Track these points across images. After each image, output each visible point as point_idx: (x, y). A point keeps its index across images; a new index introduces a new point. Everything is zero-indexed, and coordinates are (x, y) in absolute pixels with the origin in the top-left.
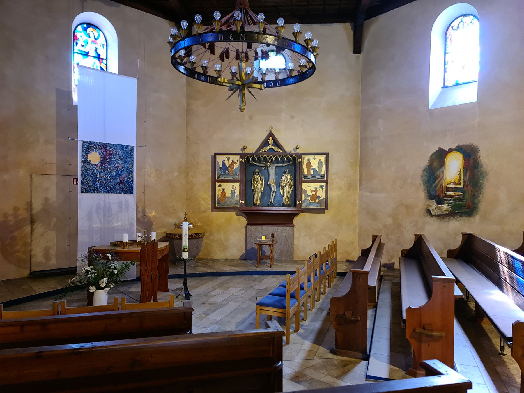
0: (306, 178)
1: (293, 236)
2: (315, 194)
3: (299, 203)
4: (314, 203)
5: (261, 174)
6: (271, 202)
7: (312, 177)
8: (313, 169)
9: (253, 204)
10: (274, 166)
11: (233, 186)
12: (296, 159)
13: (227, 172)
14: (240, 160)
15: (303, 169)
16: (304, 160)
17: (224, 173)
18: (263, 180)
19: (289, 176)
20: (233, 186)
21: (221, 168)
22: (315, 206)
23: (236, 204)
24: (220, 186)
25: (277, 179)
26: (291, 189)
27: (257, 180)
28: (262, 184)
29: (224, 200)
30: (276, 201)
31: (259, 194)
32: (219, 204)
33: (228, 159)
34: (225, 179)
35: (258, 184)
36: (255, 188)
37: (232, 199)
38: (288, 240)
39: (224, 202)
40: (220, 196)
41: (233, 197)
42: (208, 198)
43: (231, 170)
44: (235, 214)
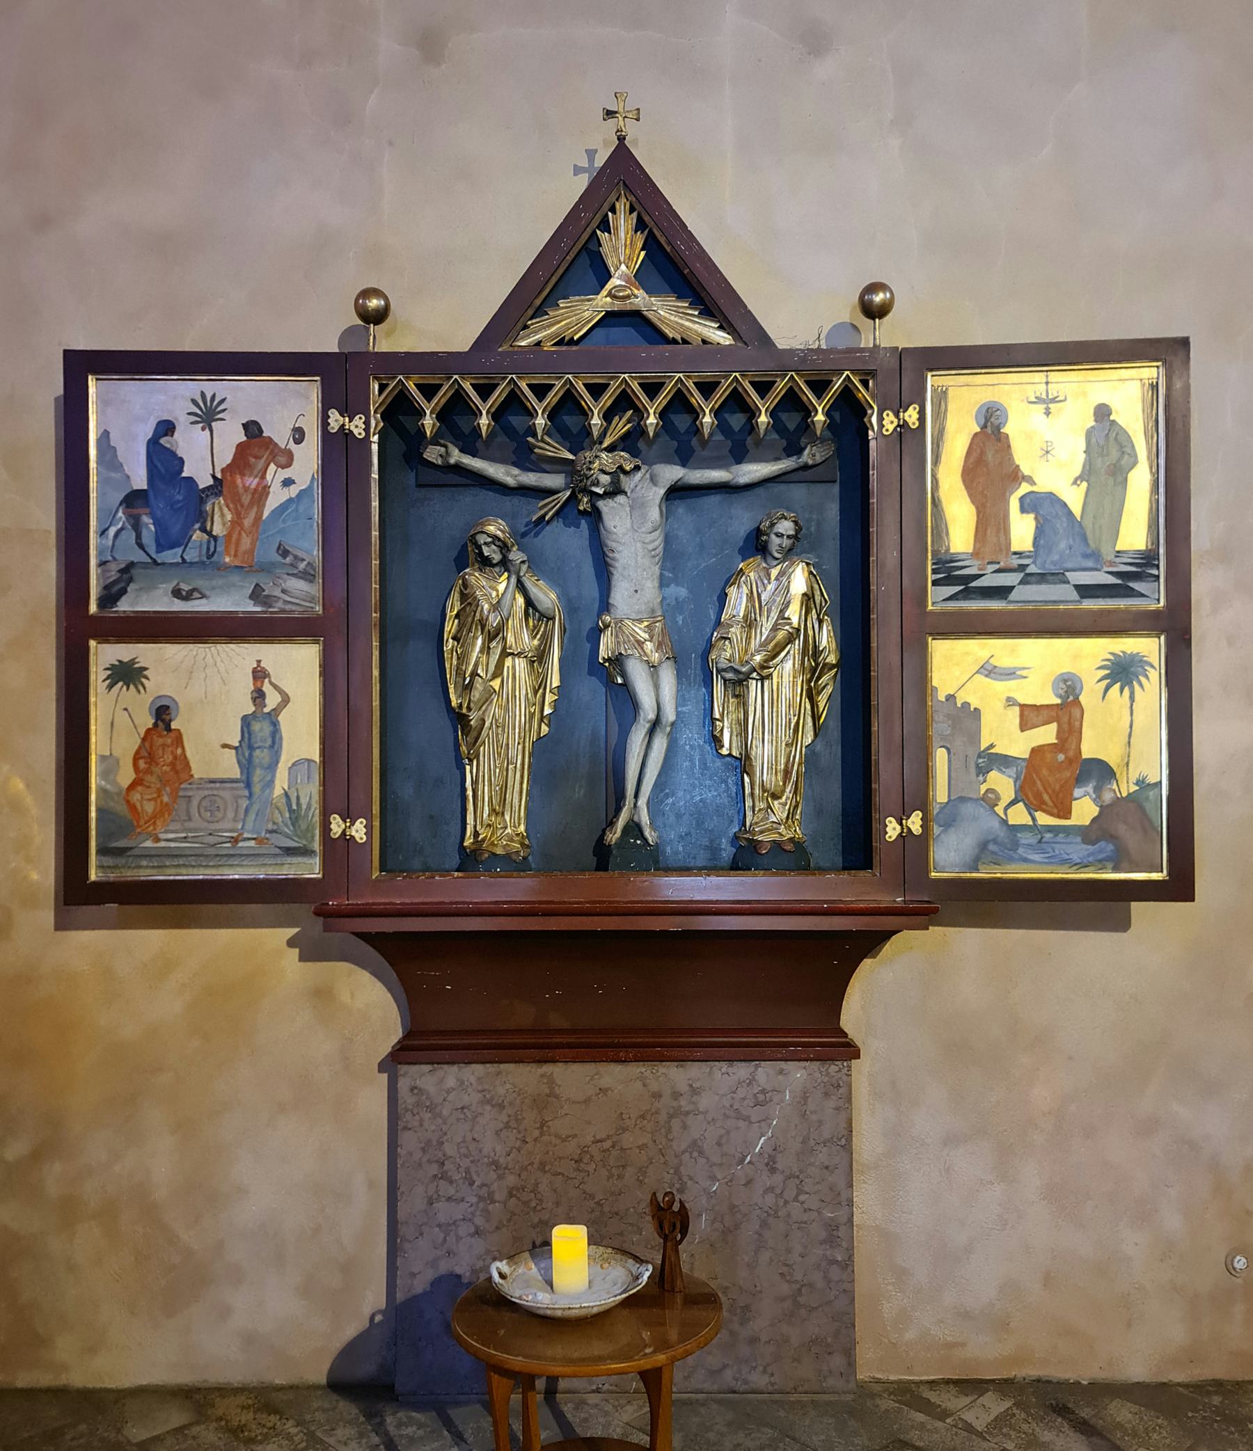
0: (967, 594)
1: (848, 1148)
2: (1060, 746)
3: (906, 836)
4: (1050, 829)
6: (634, 828)
7: (1027, 579)
9: (462, 847)
10: (654, 480)
11: (259, 674)
13: (197, 536)
15: (936, 503)
16: (940, 415)
17: (172, 547)
18: (553, 618)
19: (799, 581)
20: (259, 674)
21: (134, 499)
22: (1064, 862)
23: (289, 851)
24: (127, 674)
25: (679, 606)
27: (494, 620)
28: (540, 657)
29: (163, 811)
30: (679, 816)
31: (519, 756)
32: (121, 852)
33: (208, 415)
34: (179, 606)
35: (505, 654)
36: (476, 694)
37: (244, 803)
38: (800, 1191)
39: (169, 837)
40: (126, 776)
41: (257, 789)
42: (29, 800)
43: (237, 523)
44: (291, 943)
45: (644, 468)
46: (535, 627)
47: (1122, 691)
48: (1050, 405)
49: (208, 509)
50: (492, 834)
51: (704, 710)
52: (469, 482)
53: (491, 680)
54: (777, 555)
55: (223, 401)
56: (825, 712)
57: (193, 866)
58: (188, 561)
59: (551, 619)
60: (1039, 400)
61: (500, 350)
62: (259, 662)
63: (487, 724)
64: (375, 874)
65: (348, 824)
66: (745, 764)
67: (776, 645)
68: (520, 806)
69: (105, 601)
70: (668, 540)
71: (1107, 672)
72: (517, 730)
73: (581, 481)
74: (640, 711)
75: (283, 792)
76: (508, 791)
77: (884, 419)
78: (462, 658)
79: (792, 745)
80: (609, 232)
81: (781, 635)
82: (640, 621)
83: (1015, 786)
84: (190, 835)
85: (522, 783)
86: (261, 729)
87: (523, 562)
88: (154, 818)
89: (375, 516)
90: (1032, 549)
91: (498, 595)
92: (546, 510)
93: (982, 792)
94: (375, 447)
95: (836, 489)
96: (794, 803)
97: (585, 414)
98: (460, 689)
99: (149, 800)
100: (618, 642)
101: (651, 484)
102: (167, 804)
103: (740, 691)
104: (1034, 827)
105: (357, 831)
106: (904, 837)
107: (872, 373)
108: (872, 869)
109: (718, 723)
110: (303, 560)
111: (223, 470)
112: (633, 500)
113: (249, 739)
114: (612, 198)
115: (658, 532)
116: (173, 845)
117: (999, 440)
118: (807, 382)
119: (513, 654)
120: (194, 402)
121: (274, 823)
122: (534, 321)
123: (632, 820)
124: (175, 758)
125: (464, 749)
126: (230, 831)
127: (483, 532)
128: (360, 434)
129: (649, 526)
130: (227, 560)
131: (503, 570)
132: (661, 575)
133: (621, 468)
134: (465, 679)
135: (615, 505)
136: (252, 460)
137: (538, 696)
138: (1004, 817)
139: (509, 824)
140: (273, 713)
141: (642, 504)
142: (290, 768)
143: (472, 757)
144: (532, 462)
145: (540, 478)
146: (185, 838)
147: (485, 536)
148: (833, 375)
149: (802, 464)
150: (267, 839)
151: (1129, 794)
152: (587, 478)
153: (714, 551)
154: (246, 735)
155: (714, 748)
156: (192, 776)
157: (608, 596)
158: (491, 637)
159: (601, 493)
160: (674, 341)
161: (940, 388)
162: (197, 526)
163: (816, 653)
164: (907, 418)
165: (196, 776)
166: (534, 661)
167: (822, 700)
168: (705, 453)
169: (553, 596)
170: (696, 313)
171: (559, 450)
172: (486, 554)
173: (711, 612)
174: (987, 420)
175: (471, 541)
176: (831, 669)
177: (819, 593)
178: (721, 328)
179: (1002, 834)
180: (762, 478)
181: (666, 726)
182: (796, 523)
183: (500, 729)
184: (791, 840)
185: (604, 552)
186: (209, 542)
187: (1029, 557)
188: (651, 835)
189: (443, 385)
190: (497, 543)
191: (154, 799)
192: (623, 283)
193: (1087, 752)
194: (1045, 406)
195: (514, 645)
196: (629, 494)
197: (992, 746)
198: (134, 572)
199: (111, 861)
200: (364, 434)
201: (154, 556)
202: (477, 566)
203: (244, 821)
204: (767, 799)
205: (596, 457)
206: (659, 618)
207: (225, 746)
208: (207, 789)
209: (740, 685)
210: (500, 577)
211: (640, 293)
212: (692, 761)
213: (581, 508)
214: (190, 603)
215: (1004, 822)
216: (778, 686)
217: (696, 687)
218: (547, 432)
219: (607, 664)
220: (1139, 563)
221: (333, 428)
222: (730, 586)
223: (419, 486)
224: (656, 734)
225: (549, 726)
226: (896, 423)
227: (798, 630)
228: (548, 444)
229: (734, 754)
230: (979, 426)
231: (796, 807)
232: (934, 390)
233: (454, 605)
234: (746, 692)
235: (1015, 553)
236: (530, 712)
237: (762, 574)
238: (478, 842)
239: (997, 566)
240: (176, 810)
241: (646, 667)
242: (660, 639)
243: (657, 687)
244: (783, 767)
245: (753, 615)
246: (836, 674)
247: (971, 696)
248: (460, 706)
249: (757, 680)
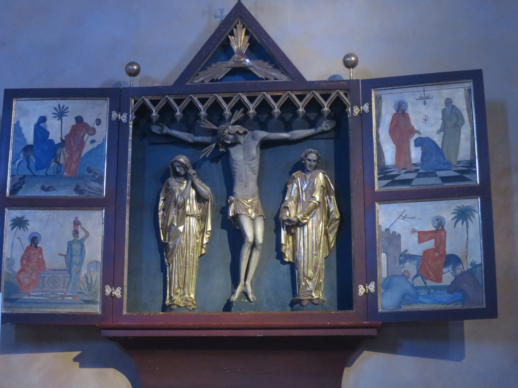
0: (394, 183)
2: (436, 249)
3: (367, 294)
4: (435, 288)
5: (199, 176)
6: (245, 294)
7: (419, 176)
8: (419, 142)
10: (253, 138)
11: (77, 223)
12: (345, 107)
13: (53, 164)
14: (110, 117)
15: (379, 144)
17: (42, 169)
18: (208, 200)
19: (320, 178)
20: (77, 223)
21: (28, 149)
23: (87, 302)
24: (20, 223)
26: (328, 237)
32: (13, 301)
34: (43, 194)
37: (68, 280)
39: (34, 294)
40: (17, 267)
41: (73, 273)
43: (71, 158)
44: (75, 360)
47: (463, 223)
48: (426, 100)
49: (58, 153)
55: (67, 108)
57: (45, 308)
58: (48, 175)
60: (421, 98)
62: (76, 218)
64: (125, 313)
69: (14, 190)
71: (455, 215)
75: (85, 275)
80: (234, 36)
83: (417, 269)
84: (44, 294)
86: (76, 247)
87: (194, 174)
88: (29, 286)
89: (130, 155)
90: (421, 162)
92: (206, 153)
93: (402, 271)
94: (131, 126)
99: (27, 278)
102: (34, 280)
104: (426, 287)
105: (117, 293)
107: (348, 90)
110: (97, 174)
111: (65, 137)
113: (71, 252)
114: (236, 22)
116: (36, 298)
117: (405, 116)
120: (55, 109)
121: (80, 289)
122: (201, 72)
124: (39, 259)
126: (62, 292)
127: (177, 161)
130: (65, 174)
136: (78, 132)
138: (412, 283)
140: (82, 240)
142: (88, 265)
146: (41, 295)
150: (77, 296)
151: (468, 270)
154: (70, 250)
156: (45, 268)
160: (262, 79)
161: (378, 96)
162: (53, 160)
163: (329, 214)
164: (364, 109)
165: (47, 268)
171: (211, 125)
174: (399, 108)
179: (411, 291)
186: (58, 166)
187: (419, 166)
190: (183, 166)
191: (29, 278)
193: (448, 251)
194: (424, 100)
195: (189, 211)
196: (242, 144)
197: (406, 251)
198: (26, 179)
199: (9, 304)
200: (126, 121)
201: (34, 172)
203: (67, 288)
207: (60, 255)
208: (52, 273)
214: (49, 192)
215: (412, 285)
220: (466, 166)
221: (113, 119)
230: (396, 110)
232: (376, 97)
235: (413, 164)
239: (405, 171)
240: (38, 283)
247: (397, 229)
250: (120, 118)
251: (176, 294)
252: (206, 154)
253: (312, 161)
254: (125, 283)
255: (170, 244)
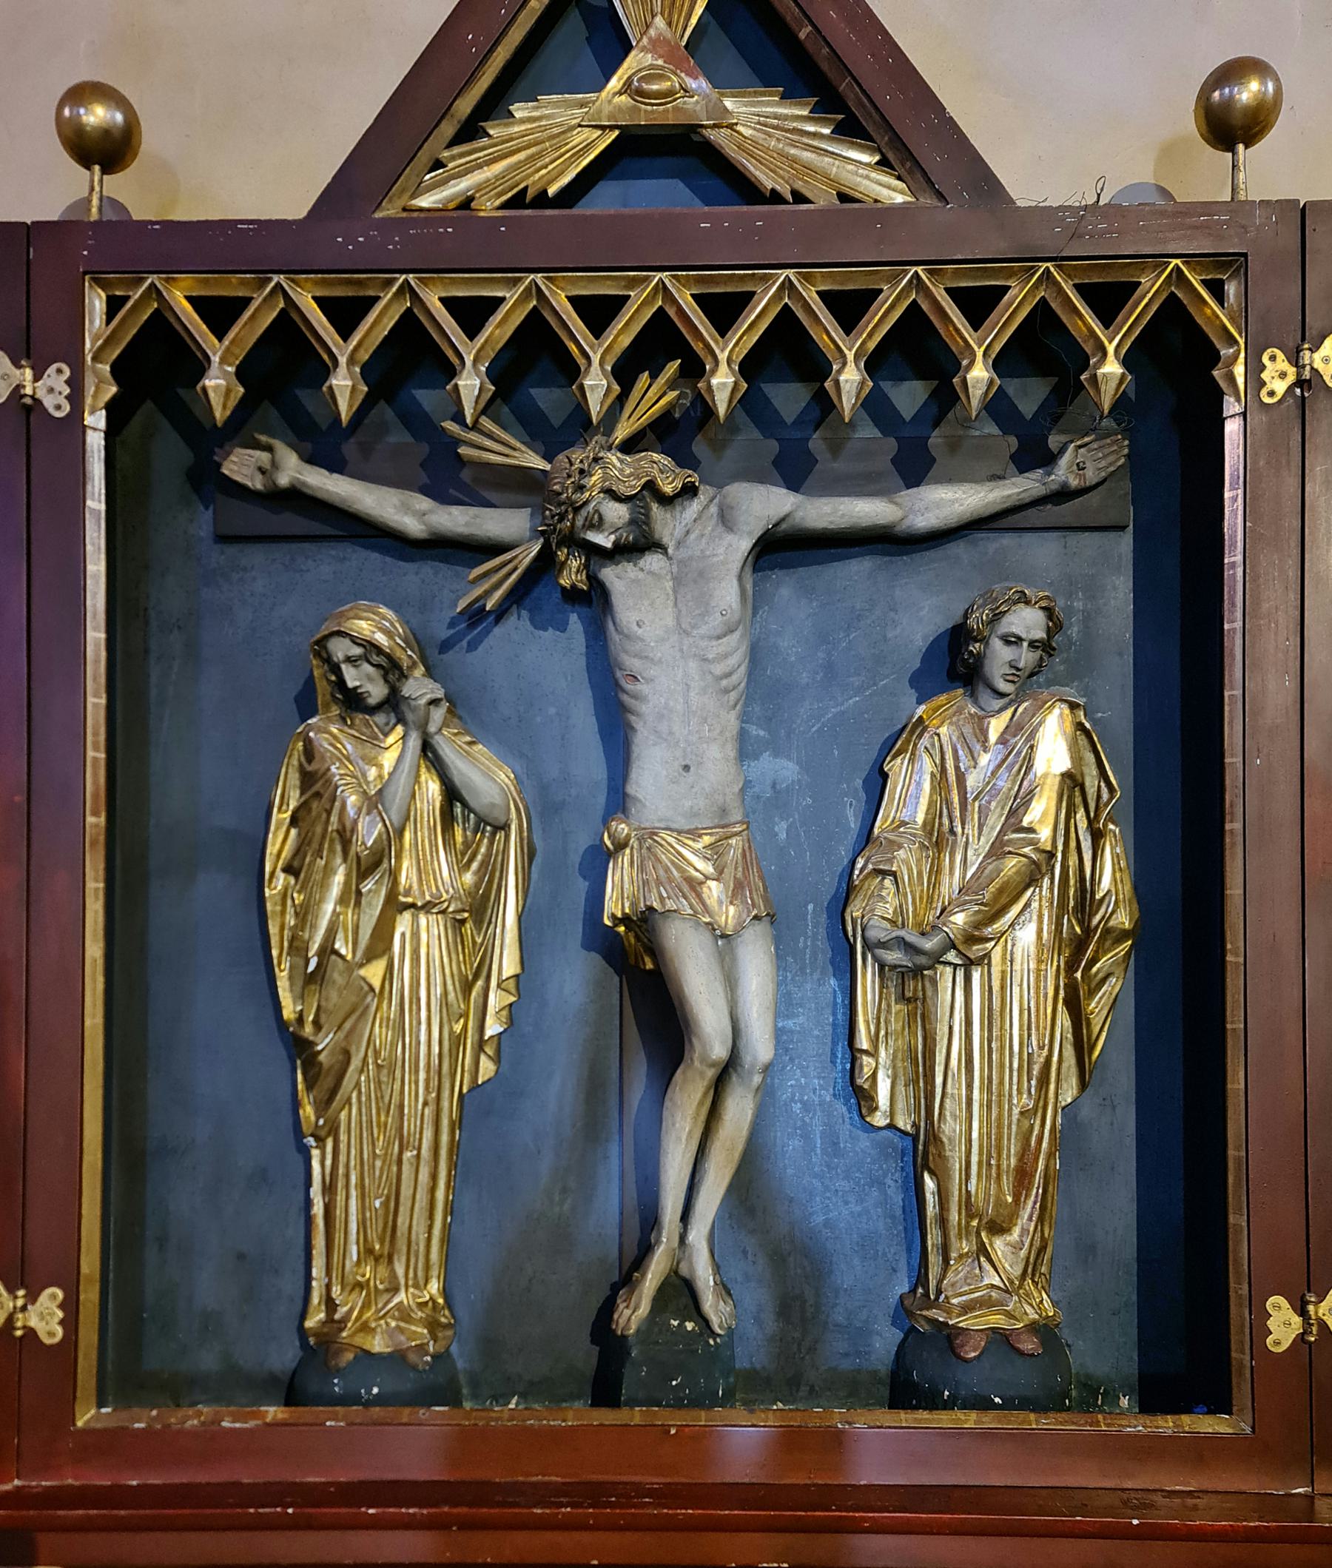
5: (456, 705)
9: (302, 1332)
10: (726, 520)
18: (505, 827)
25: (778, 800)
27: (369, 833)
35: (394, 905)
36: (334, 997)
45: (705, 492)
46: (467, 845)
50: (366, 1306)
51: (834, 1025)
52: (328, 530)
53: (361, 965)
54: (1003, 686)
56: (1104, 1034)
59: (502, 828)
61: (378, 215)
63: (355, 1063)
65: (20, 1303)
66: (926, 1152)
67: (1001, 891)
68: (429, 1240)
70: (756, 656)
72: (422, 1075)
73: (562, 517)
74: (695, 1041)
76: (401, 1209)
77: (1263, 367)
78: (305, 914)
79: (1035, 1114)
81: (1011, 865)
82: (695, 834)
85: (433, 1190)
87: (434, 702)
91: (380, 776)
94: (96, 442)
95: (1125, 543)
96: (1037, 1243)
97: (570, 371)
98: (299, 983)
100: (646, 883)
101: (721, 529)
103: (915, 990)
105: (42, 1317)
106: (1310, 1343)
107: (1234, 263)
108: (1230, 1413)
109: (866, 1060)
112: (682, 563)
115: (736, 635)
118: (1078, 288)
119: (413, 906)
122: (456, 150)
123: (676, 1272)
125: (308, 1111)
127: (340, 633)
128: (58, 407)
129: (715, 622)
131: (393, 721)
132: (742, 736)
133: (650, 486)
134: (307, 961)
135: (641, 575)
137: (474, 994)
139: (402, 1281)
141: (701, 574)
143: (323, 1133)
144: (462, 487)
145: (476, 516)
147: (347, 641)
148: (1143, 269)
149: (1054, 487)
152: (577, 510)
153: (856, 681)
155: (855, 1107)
157: (625, 777)
158: (364, 869)
159: (609, 545)
160: (776, 198)
163: (1086, 902)
166: (463, 922)
167: (1097, 1007)
168: (840, 466)
169: (504, 776)
170: (827, 131)
172: (351, 684)
173: (850, 813)
175: (317, 654)
176: (1119, 941)
177: (1095, 772)
178: (884, 163)
180: (967, 517)
181: (751, 1073)
182: (1049, 611)
183: (385, 1071)
184: (1033, 1328)
185: (617, 684)
188: (717, 1311)
189: (252, 298)
190: (375, 659)
192: (660, 62)
195: (415, 886)
196: (670, 551)
200: (67, 408)
202: (335, 711)
204: (978, 1234)
205: (596, 460)
206: (738, 828)
209: (915, 977)
210: (386, 735)
211: (699, 84)
212: (806, 1137)
213: (565, 582)
216: (1003, 979)
217: (816, 976)
218: (487, 409)
219: (622, 929)
222: (894, 757)
223: (223, 539)
224: (729, 1090)
225: (497, 1059)
226: (1291, 378)
227: (1051, 855)
228: (490, 436)
229: (901, 1124)
231: (1042, 1249)
233: (288, 795)
234: (929, 993)
236: (451, 1032)
237: (967, 730)
238: (333, 1321)
241: (706, 937)
242: (739, 875)
243: (731, 982)
244: (1013, 1161)
245: (946, 821)
246: (1128, 954)
248: (300, 1020)
249: (956, 966)
250: (34, 389)
251: (353, 1289)
252: (488, 593)
253: (1025, 644)
254: (90, 1263)
255: (320, 1048)
